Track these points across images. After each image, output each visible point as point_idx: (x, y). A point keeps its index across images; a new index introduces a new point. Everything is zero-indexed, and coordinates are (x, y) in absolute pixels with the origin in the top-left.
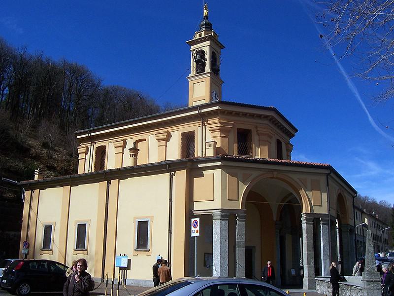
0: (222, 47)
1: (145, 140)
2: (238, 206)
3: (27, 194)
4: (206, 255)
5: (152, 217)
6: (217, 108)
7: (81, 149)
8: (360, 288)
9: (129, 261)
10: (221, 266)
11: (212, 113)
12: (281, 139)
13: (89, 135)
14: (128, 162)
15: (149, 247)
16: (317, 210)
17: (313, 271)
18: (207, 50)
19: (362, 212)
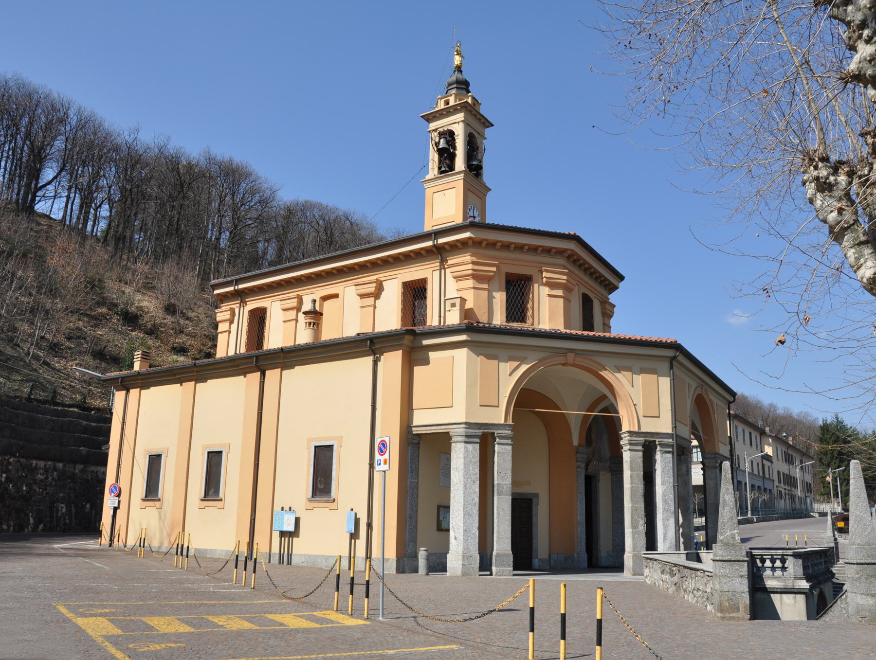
0: (488, 124)
1: (336, 296)
2: (498, 416)
3: (119, 396)
4: (441, 509)
5: (310, 440)
6: (467, 235)
7: (222, 315)
8: (709, 574)
9: (297, 520)
10: (465, 531)
11: (459, 244)
12: (591, 295)
13: (236, 288)
14: (304, 337)
15: (333, 494)
16: (649, 426)
17: (642, 541)
18: (459, 131)
19: (762, 433)
